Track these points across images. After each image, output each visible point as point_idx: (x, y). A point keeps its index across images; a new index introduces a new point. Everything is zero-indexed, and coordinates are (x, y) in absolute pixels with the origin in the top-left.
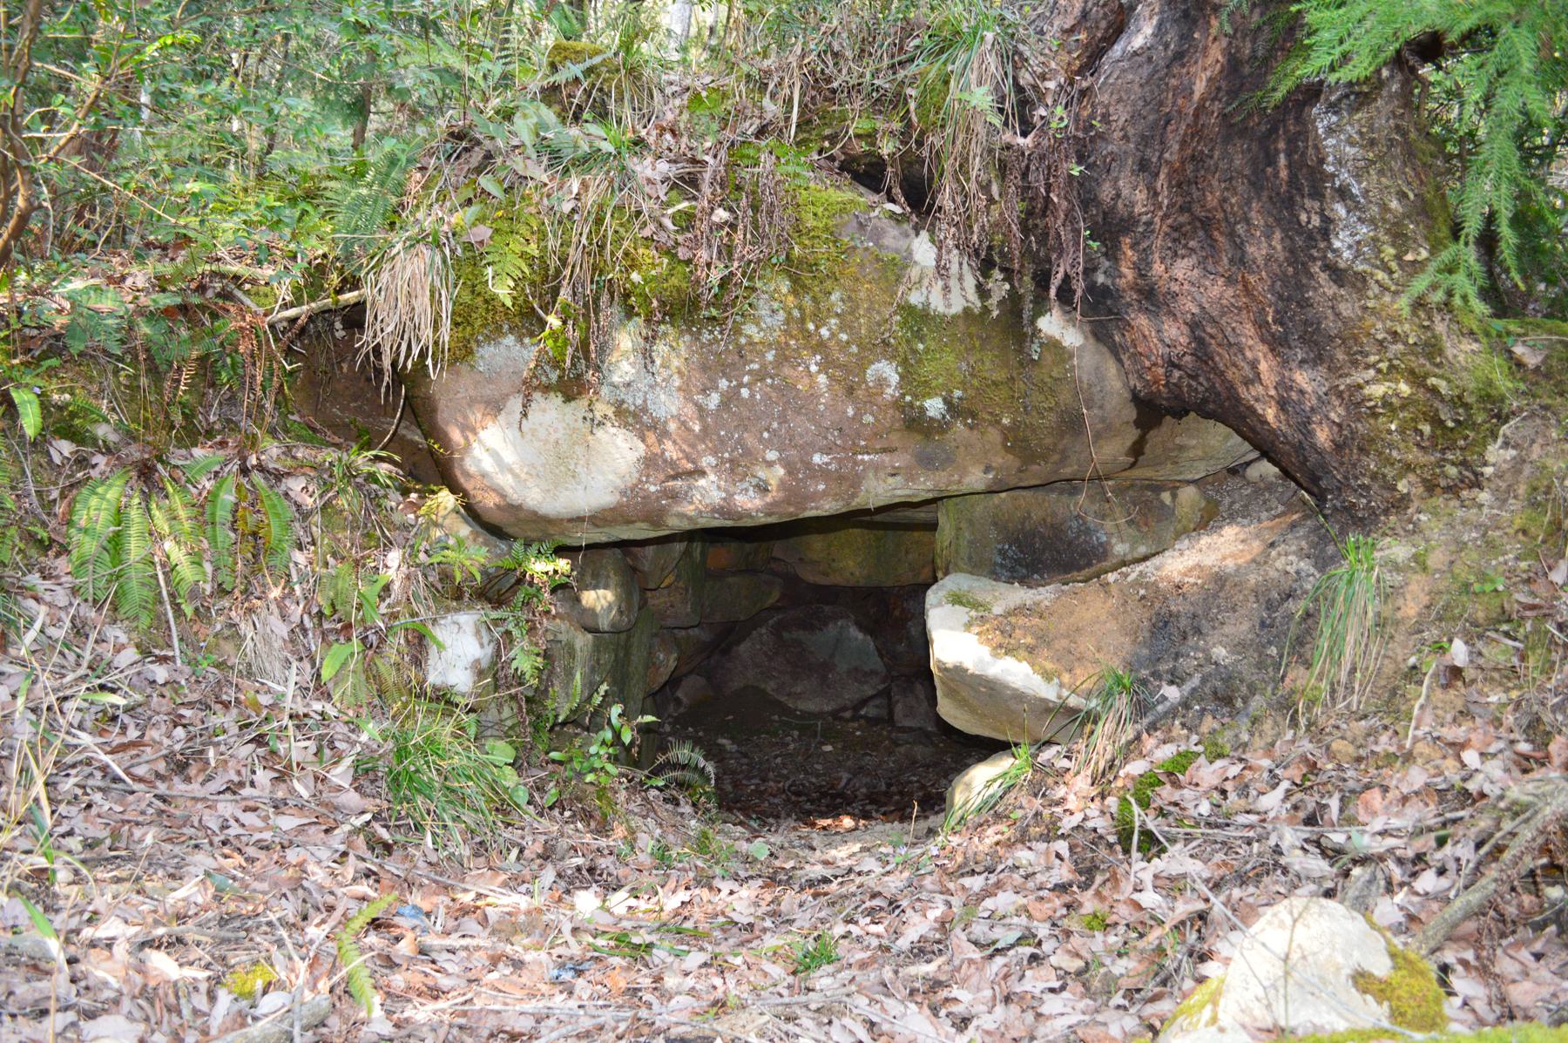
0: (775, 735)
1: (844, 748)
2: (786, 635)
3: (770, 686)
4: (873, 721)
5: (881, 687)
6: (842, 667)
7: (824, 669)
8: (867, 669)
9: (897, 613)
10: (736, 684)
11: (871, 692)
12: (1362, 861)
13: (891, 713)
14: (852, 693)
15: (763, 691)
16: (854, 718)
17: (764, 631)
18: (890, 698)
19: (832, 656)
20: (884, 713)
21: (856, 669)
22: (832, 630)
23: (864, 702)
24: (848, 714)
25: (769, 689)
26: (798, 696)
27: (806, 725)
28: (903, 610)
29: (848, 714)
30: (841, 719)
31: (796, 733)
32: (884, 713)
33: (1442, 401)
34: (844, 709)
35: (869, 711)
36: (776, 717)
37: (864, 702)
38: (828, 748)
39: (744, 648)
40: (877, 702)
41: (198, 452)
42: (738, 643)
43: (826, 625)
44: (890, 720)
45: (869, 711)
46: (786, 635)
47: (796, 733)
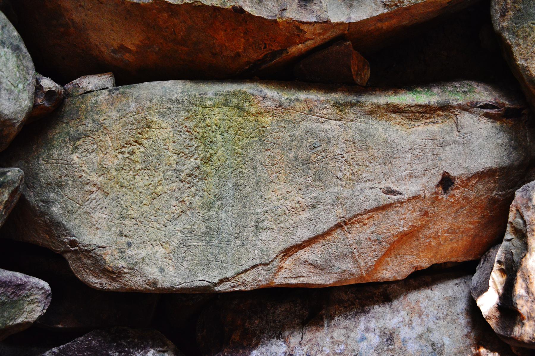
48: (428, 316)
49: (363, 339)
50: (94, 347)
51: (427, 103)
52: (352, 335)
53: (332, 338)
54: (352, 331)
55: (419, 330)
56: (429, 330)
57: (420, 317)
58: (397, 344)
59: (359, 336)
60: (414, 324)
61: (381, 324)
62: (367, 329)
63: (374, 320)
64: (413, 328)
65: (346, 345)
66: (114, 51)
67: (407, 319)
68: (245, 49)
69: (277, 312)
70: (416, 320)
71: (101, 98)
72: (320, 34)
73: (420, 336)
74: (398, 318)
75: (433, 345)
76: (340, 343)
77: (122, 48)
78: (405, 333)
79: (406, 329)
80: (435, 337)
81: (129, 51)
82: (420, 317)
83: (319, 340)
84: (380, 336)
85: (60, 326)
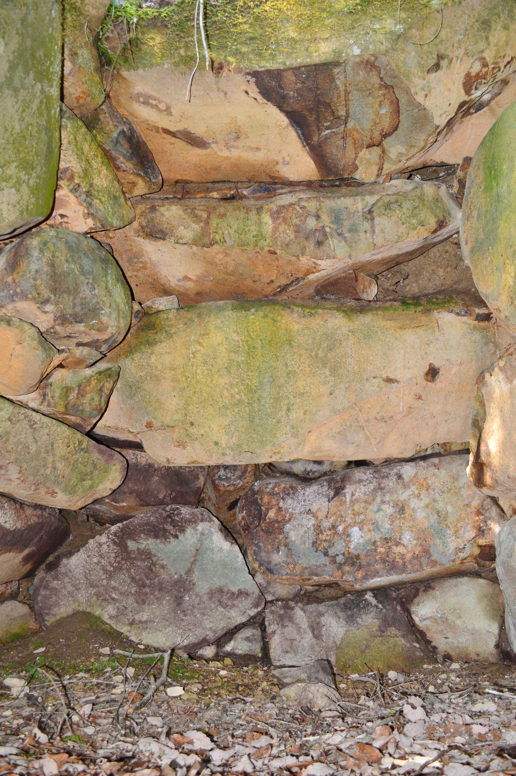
0: (100, 672)
1: (202, 692)
2: (131, 545)
3: (106, 613)
4: (241, 661)
5: (253, 612)
6: (203, 586)
7: (181, 587)
8: (235, 589)
9: (272, 514)
10: (63, 609)
11: (241, 619)
12: (208, 217)
13: (265, 649)
14: (216, 622)
15: (98, 618)
16: (217, 657)
17: (103, 539)
18: (263, 629)
19: (189, 572)
20: (256, 649)
21: (220, 590)
22: (189, 538)
23: (231, 634)
24: (209, 651)
25: (105, 618)
26: (144, 625)
27: (148, 664)
28: (280, 509)
29: (209, 651)
30: (200, 658)
31: (131, 671)
32: (256, 649)
33: (447, 752)
34: (204, 642)
35: (239, 645)
36: (106, 650)
37: (231, 634)
38: (176, 691)
39: (76, 563)
40: (247, 632)
41: (293, 539)
42: (69, 554)
43: (182, 530)
44: (266, 658)
45: (239, 645)
46: (131, 545)
47: (131, 671)
48: (434, 490)
49: (379, 510)
50: (152, 522)
51: (119, 285)
52: (370, 507)
53: (353, 510)
54: (370, 504)
55: (426, 501)
56: (434, 501)
57: (427, 490)
58: (408, 512)
59: (376, 508)
60: (422, 496)
61: (395, 497)
62: (383, 502)
63: (389, 495)
64: (421, 499)
65: (365, 515)
66: (179, 280)
67: (416, 492)
68: (277, 278)
69: (307, 493)
70: (424, 493)
71: (171, 316)
72: (330, 266)
73: (427, 506)
74: (408, 492)
75: (438, 512)
76: (359, 514)
77: (186, 278)
78: (414, 503)
79: (416, 500)
80: (440, 506)
81: (190, 280)
82: (427, 490)
83: (342, 513)
84: (393, 507)
85: (125, 504)
